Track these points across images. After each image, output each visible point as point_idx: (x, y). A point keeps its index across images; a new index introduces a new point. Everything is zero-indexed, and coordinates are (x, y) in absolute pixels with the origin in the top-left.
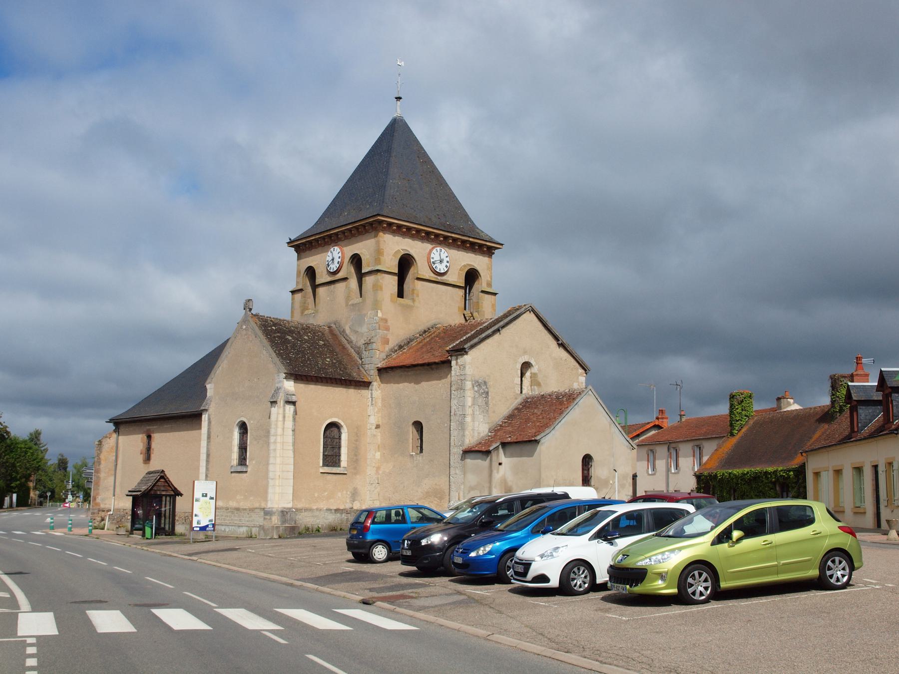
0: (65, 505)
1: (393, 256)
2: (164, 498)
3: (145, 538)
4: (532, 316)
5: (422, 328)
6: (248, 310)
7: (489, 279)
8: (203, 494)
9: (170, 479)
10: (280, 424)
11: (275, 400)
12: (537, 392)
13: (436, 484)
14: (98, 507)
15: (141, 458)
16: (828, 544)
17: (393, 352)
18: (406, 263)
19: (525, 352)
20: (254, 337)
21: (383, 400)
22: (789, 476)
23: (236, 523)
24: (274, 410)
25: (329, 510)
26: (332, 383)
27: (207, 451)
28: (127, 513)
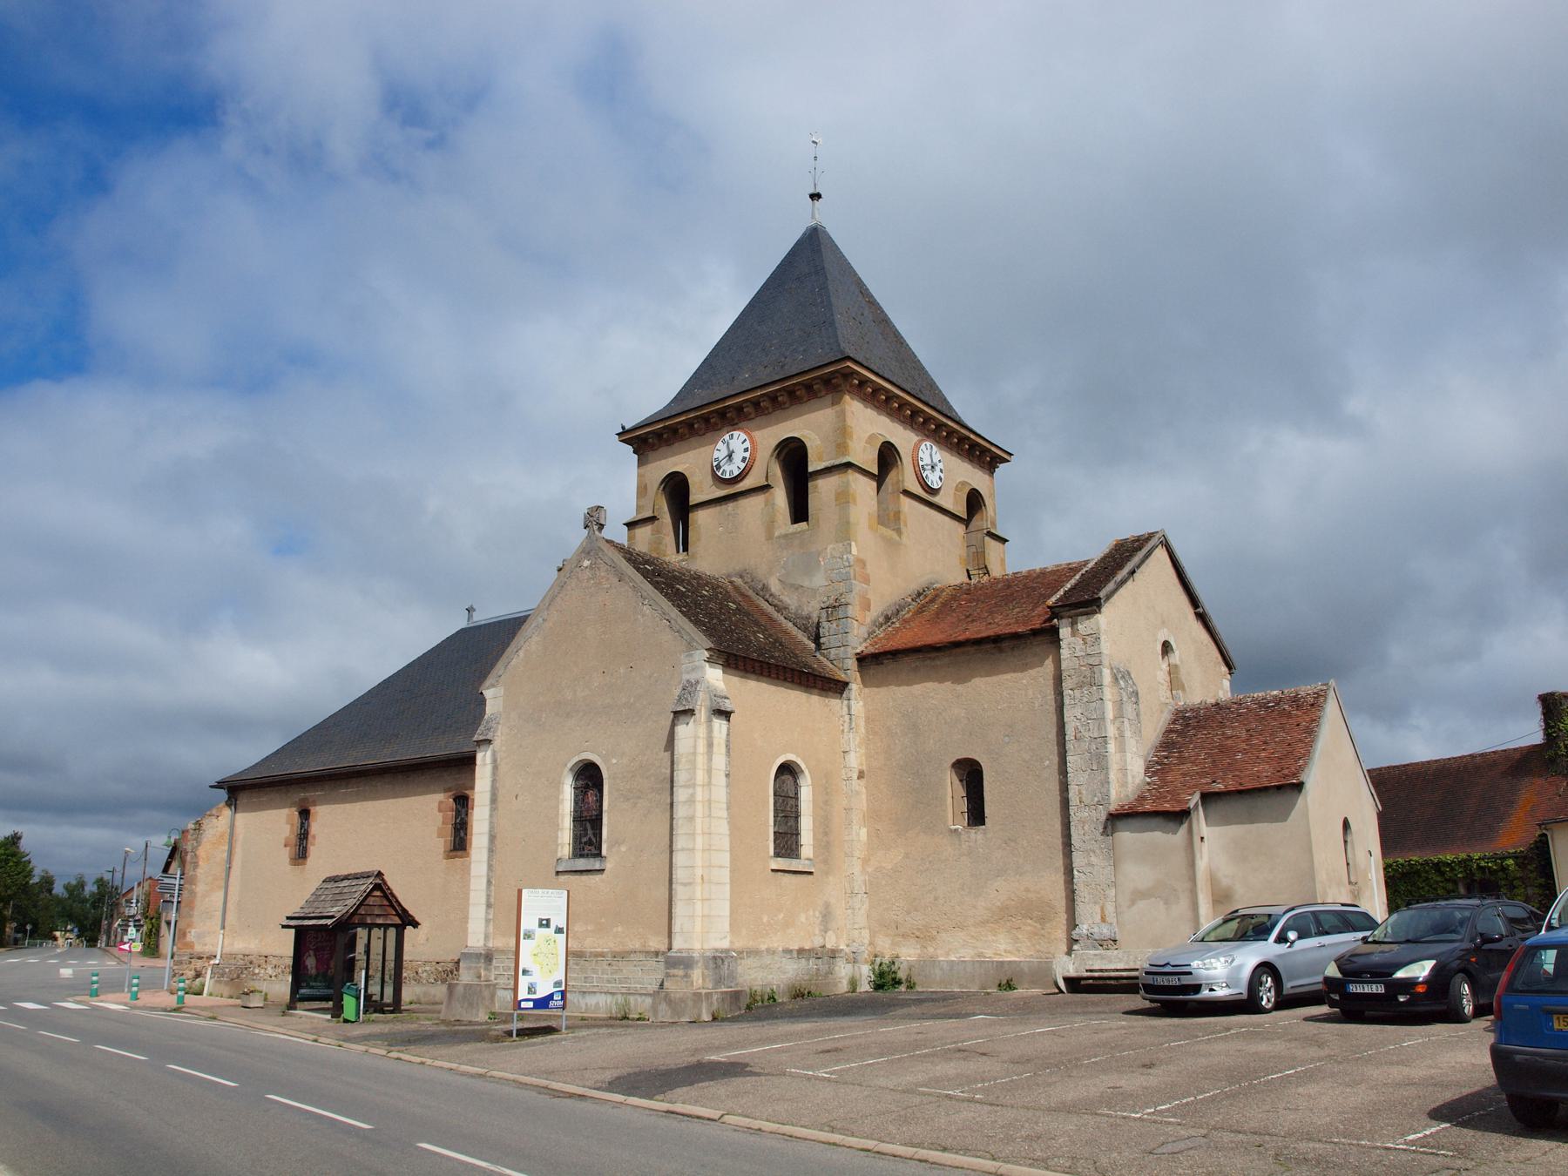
0: (122, 947)
3: (341, 1019)
5: (914, 586)
6: (596, 527)
8: (541, 920)
9: (394, 892)
10: (701, 760)
14: (189, 951)
15: (285, 854)
21: (868, 720)
22: (1504, 869)
25: (788, 951)
26: (785, 680)
28: (251, 963)
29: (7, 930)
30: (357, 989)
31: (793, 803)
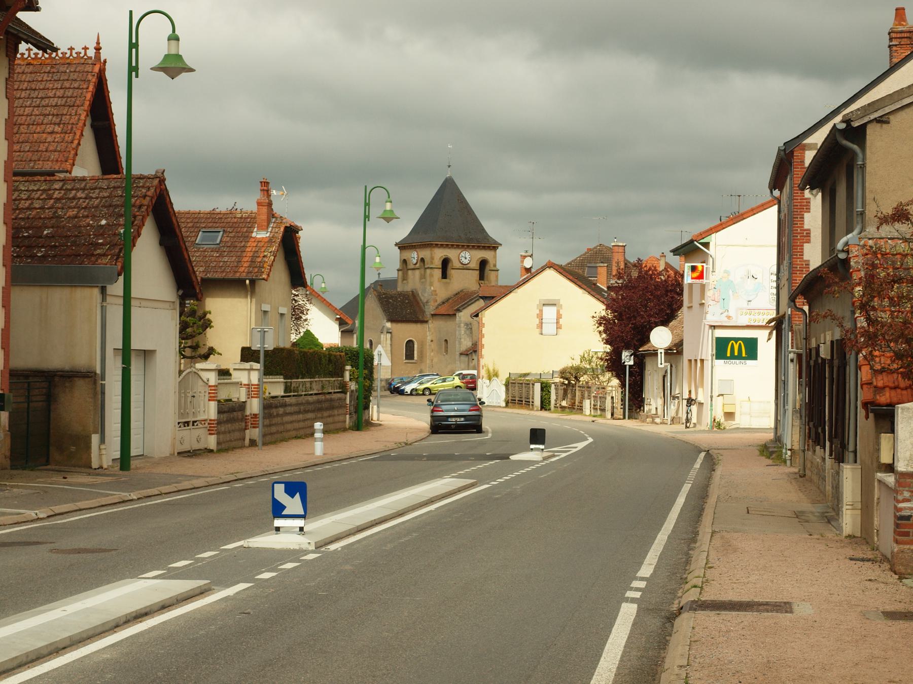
10: (385, 342)
16: (458, 385)
18: (446, 263)
24: (382, 336)
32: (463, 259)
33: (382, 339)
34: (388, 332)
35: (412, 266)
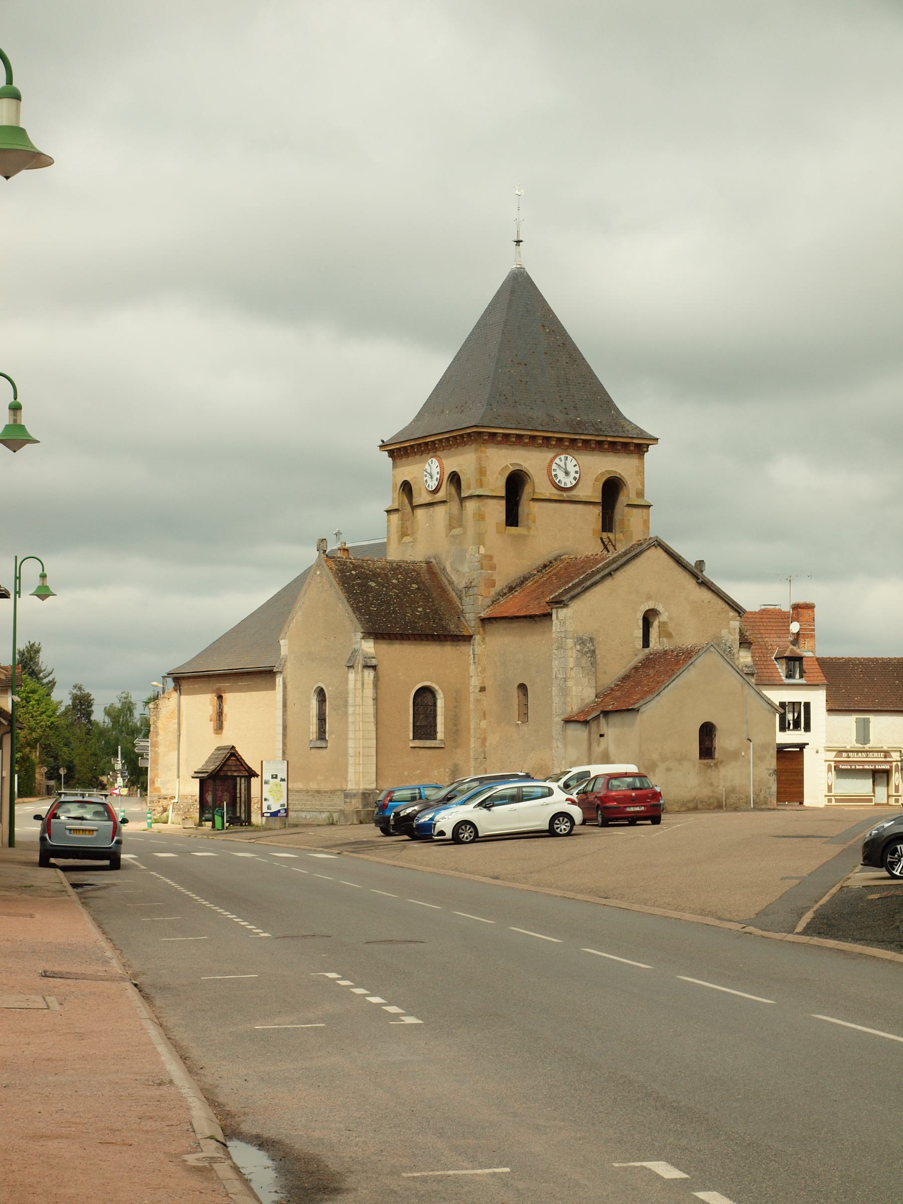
1: (499, 474)
2: (238, 779)
4: (659, 552)
7: (640, 487)
8: (272, 775)
10: (359, 692)
11: (351, 665)
12: (667, 645)
13: (541, 759)
15: (211, 726)
17: (501, 596)
19: (649, 598)
20: (329, 586)
23: (317, 809)
24: (352, 676)
26: (422, 640)
27: (283, 722)
29: (37, 776)
30: (221, 812)
31: (432, 709)
32: (561, 475)
33: (351, 684)
34: (366, 666)
35: (426, 498)
